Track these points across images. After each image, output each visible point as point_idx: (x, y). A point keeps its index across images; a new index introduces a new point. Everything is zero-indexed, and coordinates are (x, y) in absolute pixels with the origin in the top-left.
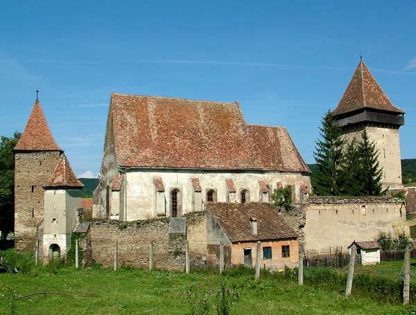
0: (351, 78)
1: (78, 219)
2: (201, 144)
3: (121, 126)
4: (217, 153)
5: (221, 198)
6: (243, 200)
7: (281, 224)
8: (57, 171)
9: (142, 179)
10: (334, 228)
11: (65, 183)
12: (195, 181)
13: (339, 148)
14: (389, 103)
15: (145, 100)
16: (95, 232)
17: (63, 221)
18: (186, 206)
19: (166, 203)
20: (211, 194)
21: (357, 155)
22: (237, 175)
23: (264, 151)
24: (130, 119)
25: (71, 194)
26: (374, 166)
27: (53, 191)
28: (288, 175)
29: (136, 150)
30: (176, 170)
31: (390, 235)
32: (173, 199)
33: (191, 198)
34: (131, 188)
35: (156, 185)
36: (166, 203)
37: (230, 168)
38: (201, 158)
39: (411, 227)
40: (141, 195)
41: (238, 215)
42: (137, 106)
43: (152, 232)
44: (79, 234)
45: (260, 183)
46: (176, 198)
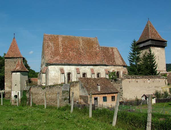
0: (145, 28)
1: (26, 85)
2: (80, 54)
3: (47, 47)
4: (87, 58)
5: (89, 76)
6: (98, 76)
7: (112, 87)
8: (17, 65)
9: (55, 68)
10: (135, 89)
11: (20, 70)
12: (77, 69)
13: (138, 55)
14: (160, 37)
15: (58, 36)
16: (33, 90)
17: (19, 85)
18: (74, 79)
19: (65, 78)
20: (84, 74)
21: (147, 58)
22: (95, 67)
23: (107, 57)
24: (51, 44)
25: (22, 74)
26: (154, 63)
27: (15, 73)
28: (117, 67)
29: (53, 57)
30: (69, 65)
31: (160, 92)
32: (68, 77)
33: (76, 76)
34: (50, 72)
35: (61, 71)
36: (65, 78)
37: (92, 64)
38: (80, 60)
39: (169, 88)
40: (55, 74)
41: (93, 83)
42: (54, 39)
43: (56, 90)
44: (26, 91)
45: (105, 70)
46: (70, 77)
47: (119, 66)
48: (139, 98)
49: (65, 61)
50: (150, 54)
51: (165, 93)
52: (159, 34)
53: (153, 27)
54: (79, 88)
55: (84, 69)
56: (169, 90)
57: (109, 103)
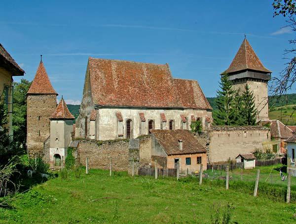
0: (239, 49)
1: (71, 139)
2: (145, 91)
6: (171, 127)
12: (141, 114)
15: (110, 62)
17: (62, 139)
23: (183, 96)
24: (101, 75)
25: (67, 123)
26: (252, 106)
28: (198, 111)
29: (105, 95)
30: (130, 108)
33: (139, 125)
35: (118, 117)
37: (163, 106)
40: (108, 124)
41: (170, 138)
42: (105, 66)
44: (73, 148)
45: (182, 116)
47: (201, 109)
48: (233, 158)
49: (123, 101)
50: (246, 94)
51: (268, 152)
52: (260, 61)
53: (253, 49)
54: (152, 145)
55: (151, 115)
56: (272, 147)
57: (194, 168)
